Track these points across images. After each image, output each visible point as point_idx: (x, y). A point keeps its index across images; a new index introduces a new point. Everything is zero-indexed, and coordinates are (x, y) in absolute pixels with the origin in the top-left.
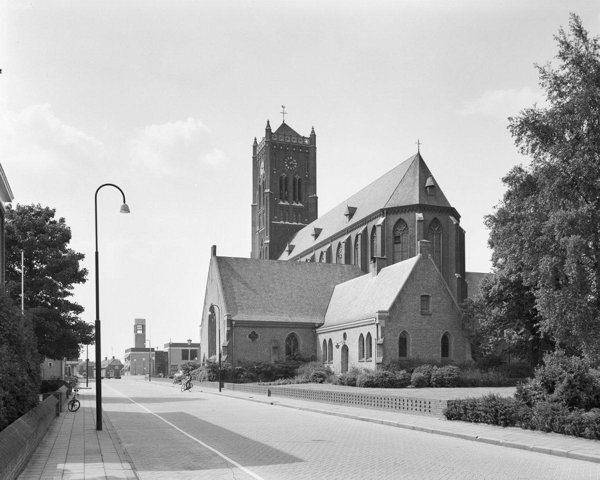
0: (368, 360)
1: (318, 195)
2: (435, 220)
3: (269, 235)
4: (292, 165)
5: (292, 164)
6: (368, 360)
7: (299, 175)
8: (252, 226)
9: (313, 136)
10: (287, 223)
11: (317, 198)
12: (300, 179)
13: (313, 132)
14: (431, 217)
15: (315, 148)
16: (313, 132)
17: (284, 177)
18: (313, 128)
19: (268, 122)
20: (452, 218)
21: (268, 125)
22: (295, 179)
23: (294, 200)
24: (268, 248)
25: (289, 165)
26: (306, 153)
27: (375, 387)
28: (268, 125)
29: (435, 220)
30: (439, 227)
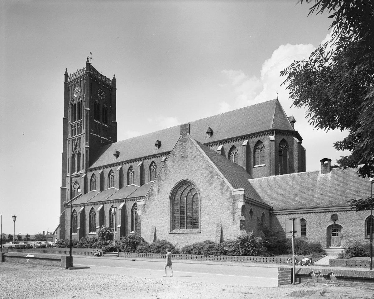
0: (171, 232)
1: (117, 121)
2: (284, 141)
3: (89, 142)
4: (102, 96)
5: (102, 95)
6: (171, 232)
7: (106, 105)
8: (64, 134)
9: (114, 81)
10: (98, 136)
11: (116, 123)
12: (106, 108)
13: (114, 78)
14: (281, 138)
15: (116, 89)
16: (114, 78)
17: (97, 103)
18: (114, 75)
19: (66, 70)
20: (296, 139)
21: (66, 72)
22: (103, 106)
23: (103, 122)
24: (88, 151)
25: (100, 95)
26: (110, 90)
27: (60, 233)
28: (66, 72)
29: (284, 141)
30: (286, 146)
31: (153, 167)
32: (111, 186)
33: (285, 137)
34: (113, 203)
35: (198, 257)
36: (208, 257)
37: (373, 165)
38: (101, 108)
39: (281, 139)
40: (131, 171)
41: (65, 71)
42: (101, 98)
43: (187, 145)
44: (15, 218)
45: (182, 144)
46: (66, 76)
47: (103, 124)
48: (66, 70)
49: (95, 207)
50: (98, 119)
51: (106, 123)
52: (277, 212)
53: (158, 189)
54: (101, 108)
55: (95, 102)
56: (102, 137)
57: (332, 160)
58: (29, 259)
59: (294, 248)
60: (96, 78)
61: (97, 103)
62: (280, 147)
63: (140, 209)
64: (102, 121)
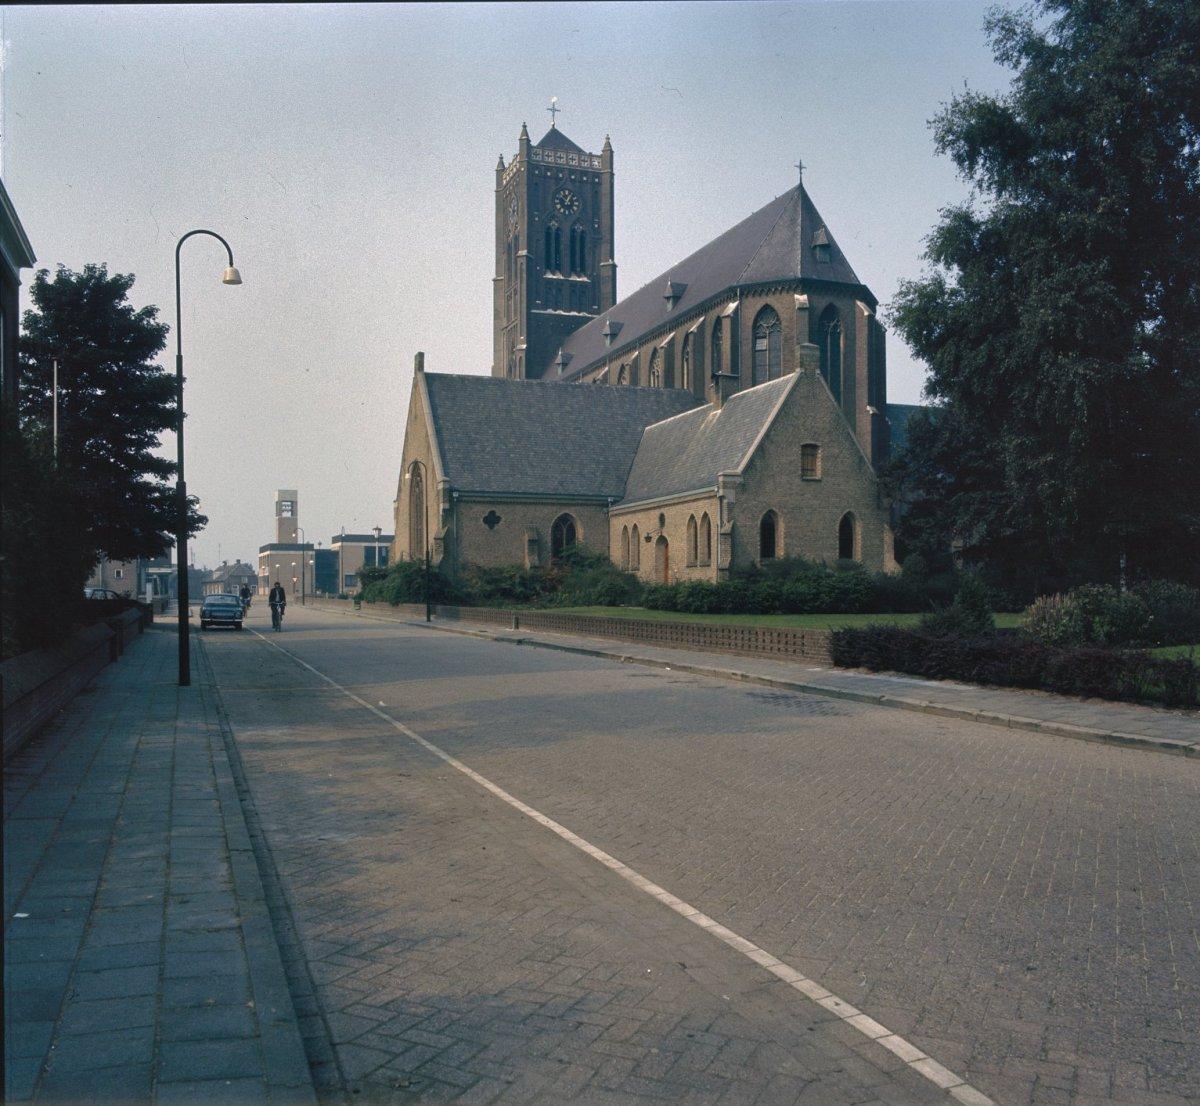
12: (583, 232)
13: (608, 144)
14: (822, 302)
17: (554, 229)
19: (525, 127)
21: (525, 132)
22: (573, 231)
23: (573, 270)
24: (524, 358)
25: (563, 206)
28: (525, 132)
29: (830, 312)
37: (2, 558)
38: (565, 241)
41: (521, 128)
48: (525, 127)
50: (557, 268)
52: (686, 496)
54: (565, 241)
56: (570, 311)
57: (291, 487)
61: (554, 229)
64: (568, 269)
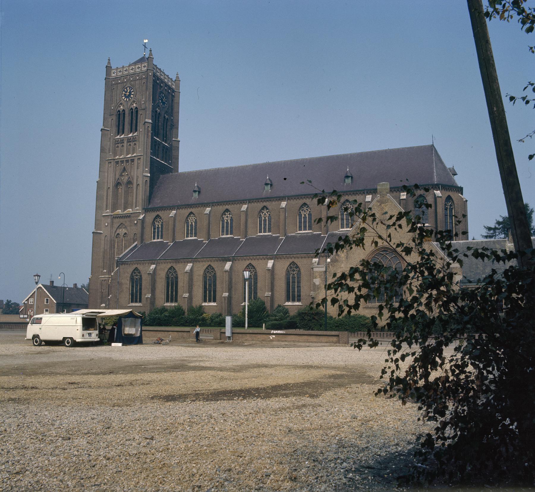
9: (177, 81)
13: (177, 77)
17: (158, 112)
22: (164, 117)
28: (109, 63)
31: (264, 214)
32: (191, 233)
33: (450, 193)
34: (210, 262)
35: (382, 334)
36: (356, 334)
39: (446, 196)
40: (227, 217)
42: (132, 94)
43: (387, 207)
44: (38, 277)
45: (380, 204)
46: (108, 68)
47: (163, 143)
49: (178, 267)
51: (166, 143)
53: (345, 254)
55: (156, 111)
58: (274, 336)
59: (245, 322)
60: (158, 79)
62: (446, 205)
63: (318, 277)
